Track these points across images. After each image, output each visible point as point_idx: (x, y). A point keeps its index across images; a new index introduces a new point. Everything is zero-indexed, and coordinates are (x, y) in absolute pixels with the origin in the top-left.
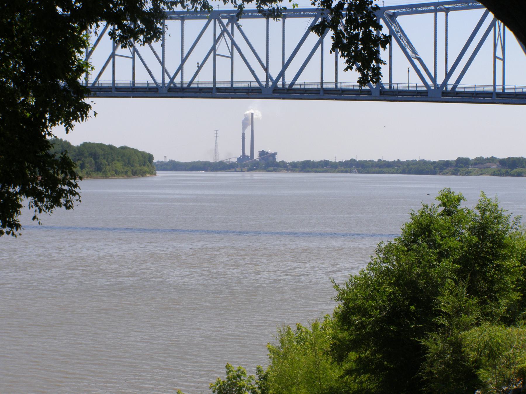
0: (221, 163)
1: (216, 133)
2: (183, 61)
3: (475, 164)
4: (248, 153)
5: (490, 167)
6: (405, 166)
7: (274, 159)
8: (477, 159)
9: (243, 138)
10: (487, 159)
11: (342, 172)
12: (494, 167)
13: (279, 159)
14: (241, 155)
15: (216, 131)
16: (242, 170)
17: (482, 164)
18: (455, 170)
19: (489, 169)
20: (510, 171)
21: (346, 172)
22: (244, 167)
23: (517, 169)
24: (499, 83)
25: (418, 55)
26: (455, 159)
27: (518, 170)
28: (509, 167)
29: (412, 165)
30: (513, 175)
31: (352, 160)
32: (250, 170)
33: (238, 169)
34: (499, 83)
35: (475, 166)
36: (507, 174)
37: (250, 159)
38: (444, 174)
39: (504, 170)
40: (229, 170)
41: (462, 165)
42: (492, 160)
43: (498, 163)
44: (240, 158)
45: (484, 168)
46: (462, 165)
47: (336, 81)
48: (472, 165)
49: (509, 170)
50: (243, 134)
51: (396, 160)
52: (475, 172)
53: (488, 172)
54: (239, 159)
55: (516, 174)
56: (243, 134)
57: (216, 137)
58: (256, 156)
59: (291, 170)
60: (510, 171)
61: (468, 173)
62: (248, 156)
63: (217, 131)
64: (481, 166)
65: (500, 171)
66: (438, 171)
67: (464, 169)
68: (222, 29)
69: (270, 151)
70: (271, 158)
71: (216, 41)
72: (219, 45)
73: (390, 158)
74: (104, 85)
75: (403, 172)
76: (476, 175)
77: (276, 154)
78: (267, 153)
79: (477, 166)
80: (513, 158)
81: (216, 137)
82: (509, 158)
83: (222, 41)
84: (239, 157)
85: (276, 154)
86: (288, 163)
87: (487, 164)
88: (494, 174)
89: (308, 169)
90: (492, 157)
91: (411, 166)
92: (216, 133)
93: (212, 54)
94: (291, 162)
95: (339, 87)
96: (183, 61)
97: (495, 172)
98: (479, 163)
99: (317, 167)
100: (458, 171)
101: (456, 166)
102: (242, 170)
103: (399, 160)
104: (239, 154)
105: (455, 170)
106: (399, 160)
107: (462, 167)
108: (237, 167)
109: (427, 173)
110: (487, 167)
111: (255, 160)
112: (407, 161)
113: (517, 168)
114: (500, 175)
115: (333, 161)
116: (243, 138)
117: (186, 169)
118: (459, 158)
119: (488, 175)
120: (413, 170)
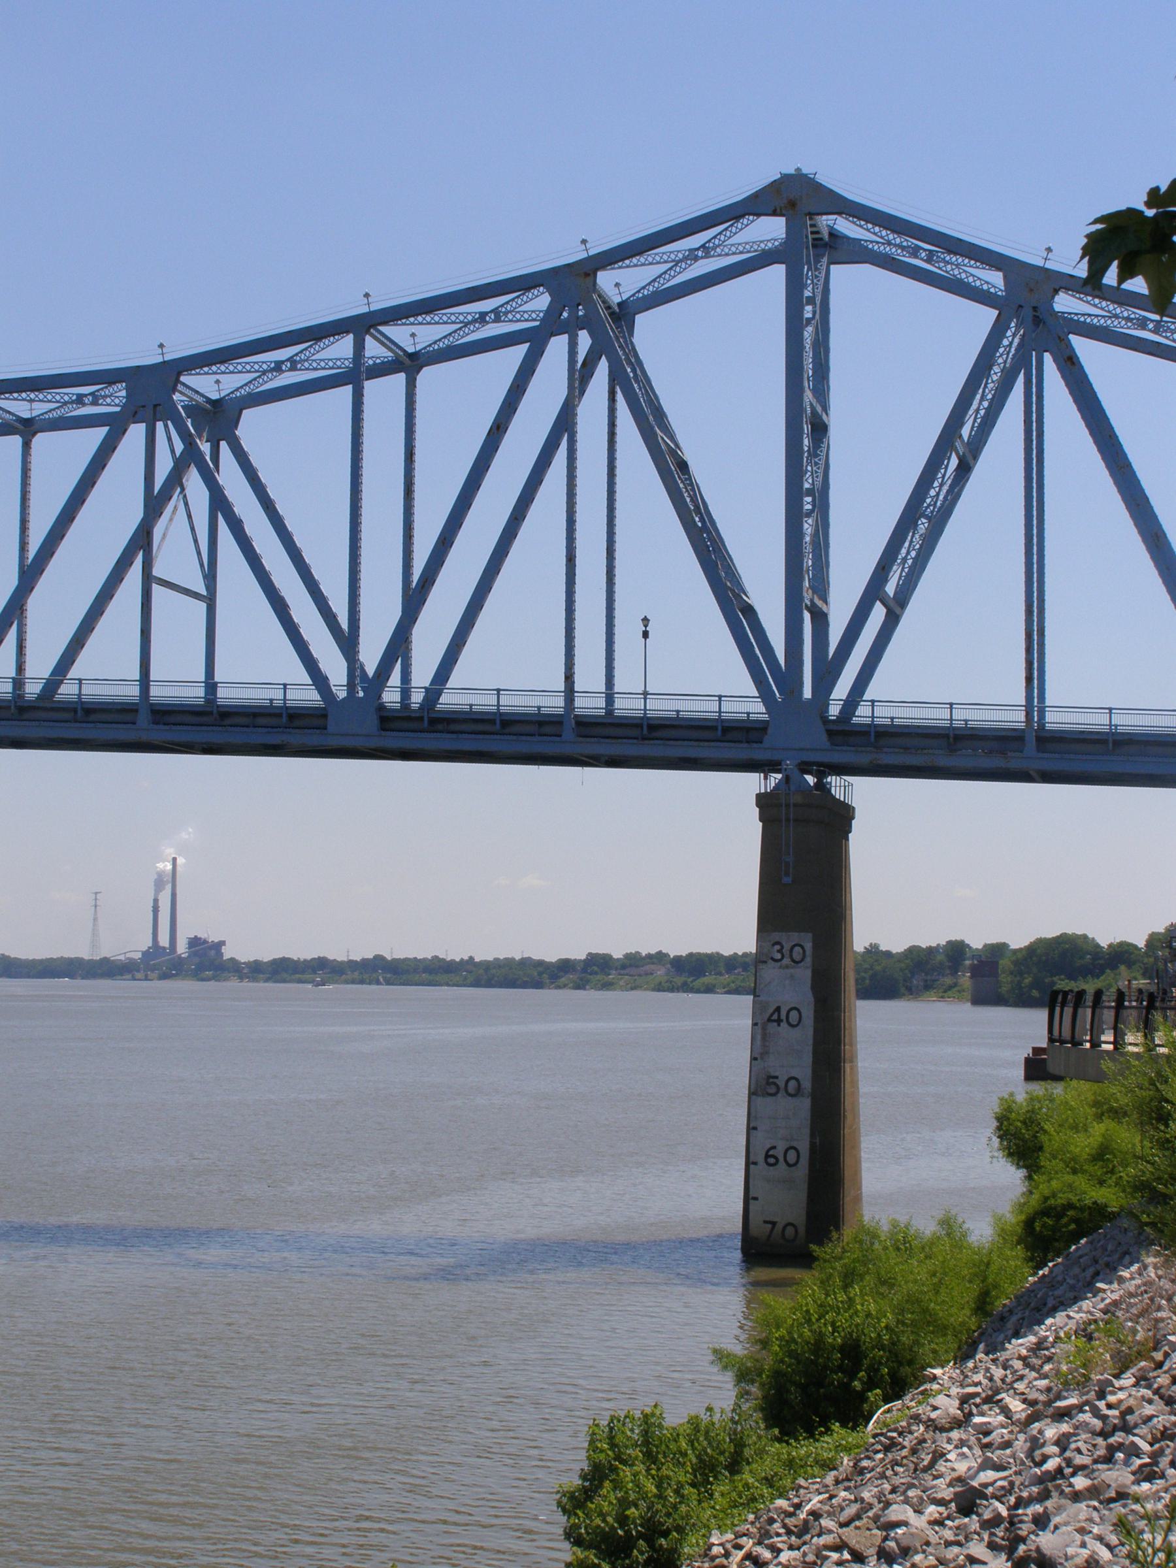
0: (105, 961)
1: (96, 899)
2: (30, 574)
3: (624, 967)
4: (164, 941)
5: (652, 974)
6: (481, 971)
7: (220, 954)
8: (628, 956)
9: (156, 910)
10: (649, 956)
11: (353, 982)
12: (660, 972)
13: (228, 953)
14: (150, 945)
15: (96, 893)
16: (146, 976)
17: (637, 967)
18: (581, 979)
19: (651, 977)
20: (692, 982)
21: (362, 982)
22: (153, 971)
23: (706, 978)
24: (590, 679)
25: (826, 602)
26: (582, 956)
27: (707, 979)
28: (691, 974)
29: (494, 968)
30: (698, 991)
31: (379, 958)
32: (164, 976)
33: (139, 975)
34: (590, 679)
35: (622, 972)
36: (686, 988)
37: (169, 954)
38: (558, 987)
39: (679, 980)
40: (120, 977)
41: (595, 968)
42: (660, 957)
43: (669, 966)
44: (147, 951)
45: (640, 975)
46: (595, 968)
47: (569, 678)
48: (616, 969)
49: (690, 980)
50: (156, 901)
51: (466, 958)
52: (622, 983)
53: (647, 983)
54: (145, 954)
55: (702, 989)
56: (156, 901)
57: (96, 906)
58: (182, 948)
59: (248, 977)
60: (692, 982)
61: (607, 986)
62: (164, 948)
63: (98, 895)
64: (633, 971)
65: (671, 982)
66: (548, 981)
67: (599, 977)
68: (179, 447)
69: (214, 938)
70: (213, 953)
71: (154, 505)
72: (164, 536)
73: (455, 954)
74: (1120, 730)
75: (477, 984)
76: (622, 989)
77: (223, 943)
78: (205, 942)
79: (625, 972)
80: (699, 954)
81: (96, 906)
82: (691, 955)
83: (173, 511)
84: (145, 949)
85: (223, 943)
86: (244, 963)
87: (648, 968)
88: (659, 988)
89: (285, 975)
90: (660, 953)
91: (494, 971)
92: (96, 899)
93: (135, 574)
94: (251, 960)
95: (576, 694)
96: (30, 574)
97: (660, 983)
98: (631, 966)
99: (303, 972)
100: (588, 981)
101: (584, 970)
102: (146, 976)
103: (471, 958)
104: (146, 943)
105: (581, 979)
106: (471, 958)
107: (596, 973)
108: (138, 971)
109: (524, 985)
110: (647, 974)
111: (179, 957)
112: (496, 959)
113: (705, 976)
114: (672, 990)
115: (345, 959)
116: (156, 910)
117: (493, 982)
118: (590, 954)
119: (646, 989)
120: (496, 979)
